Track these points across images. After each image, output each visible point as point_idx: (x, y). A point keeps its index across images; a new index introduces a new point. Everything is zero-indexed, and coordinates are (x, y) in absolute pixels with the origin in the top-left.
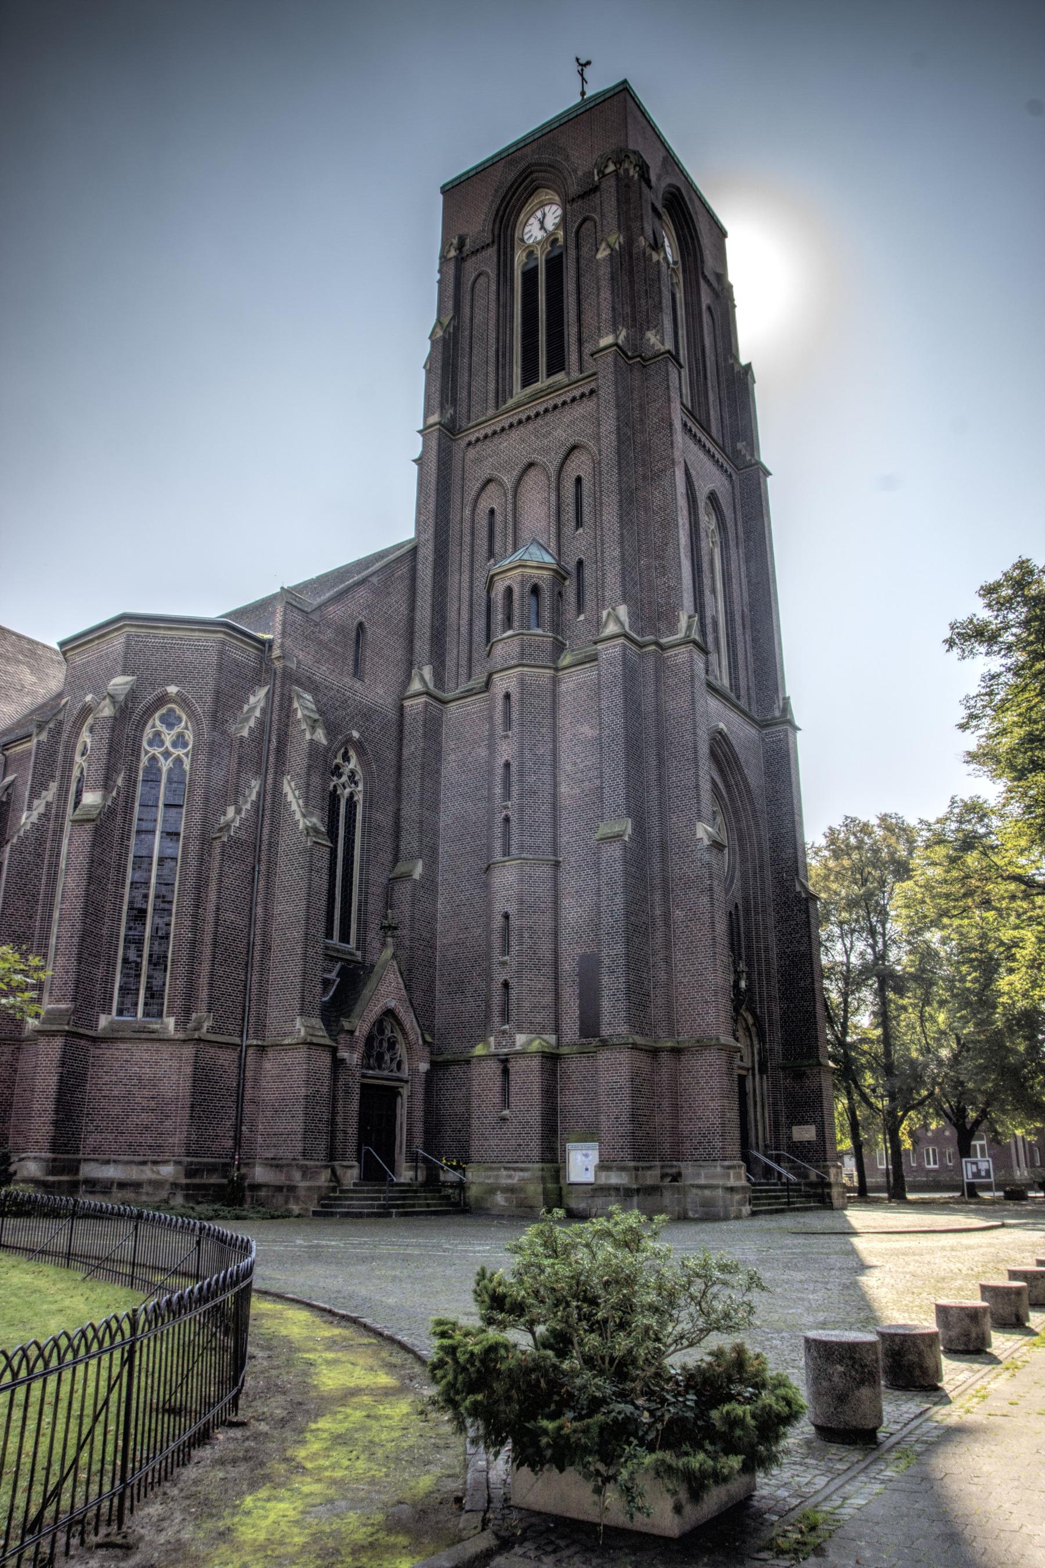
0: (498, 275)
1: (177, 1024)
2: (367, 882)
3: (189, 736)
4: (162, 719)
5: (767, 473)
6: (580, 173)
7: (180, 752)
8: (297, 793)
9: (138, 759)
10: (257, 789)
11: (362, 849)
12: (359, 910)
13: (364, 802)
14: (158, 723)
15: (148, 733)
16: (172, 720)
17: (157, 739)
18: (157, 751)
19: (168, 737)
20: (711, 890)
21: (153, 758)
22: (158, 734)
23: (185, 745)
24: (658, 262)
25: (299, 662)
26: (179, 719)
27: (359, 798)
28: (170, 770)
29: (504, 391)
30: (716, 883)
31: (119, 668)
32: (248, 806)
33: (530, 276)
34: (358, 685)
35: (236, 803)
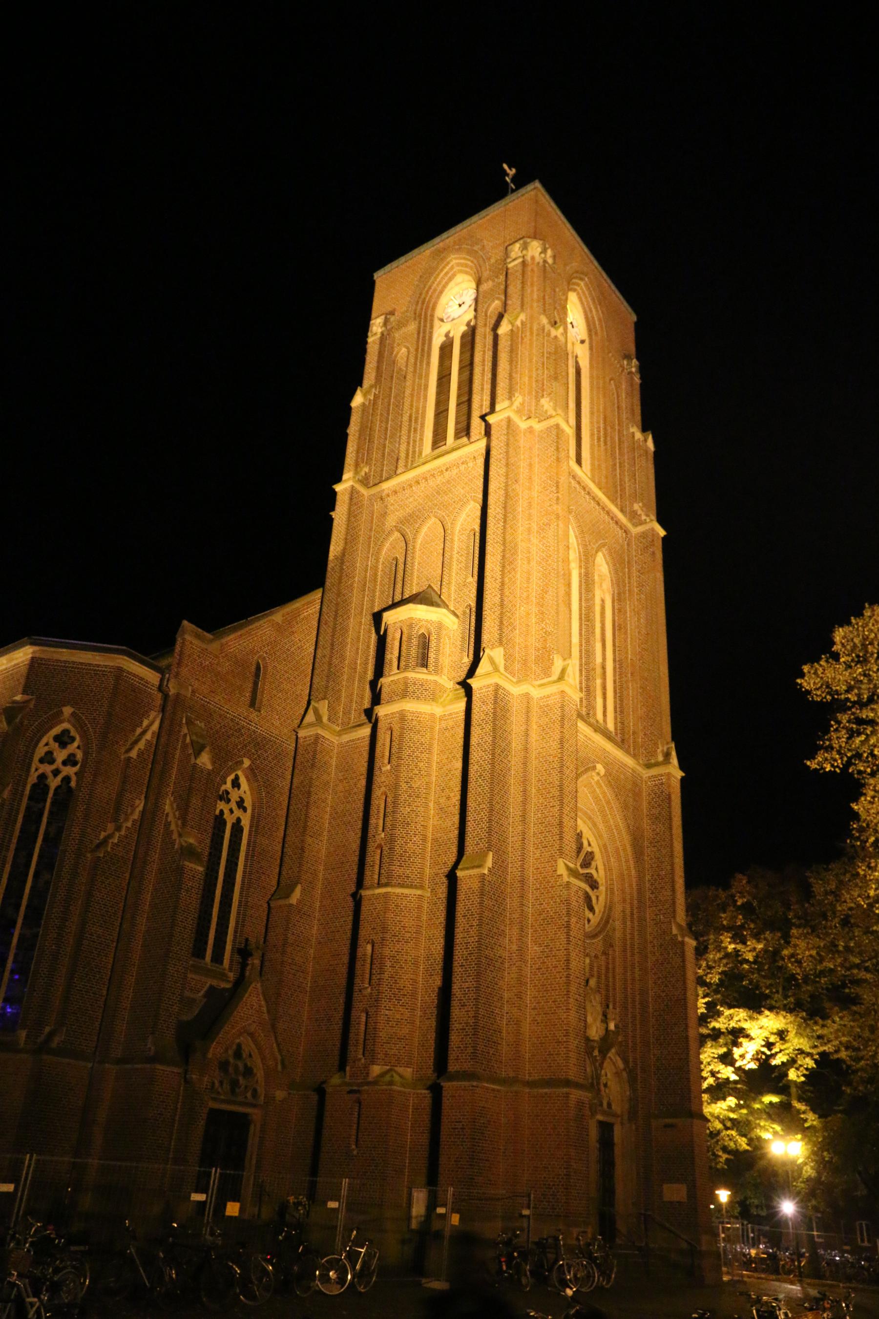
0: (417, 350)
1: (28, 1036)
2: (246, 905)
3: (79, 756)
4: (57, 738)
5: (361, 386)
6: (493, 261)
7: (70, 771)
8: (177, 813)
9: (28, 775)
10: (141, 808)
11: (244, 872)
12: (236, 932)
13: (251, 827)
14: (51, 741)
15: (41, 751)
16: (65, 739)
17: (48, 758)
18: (47, 769)
19: (61, 755)
20: (568, 926)
21: (222, 811)
22: (50, 753)
23: (75, 764)
24: (556, 337)
25: (193, 691)
26: (73, 739)
27: (246, 823)
28: (58, 788)
29: (414, 452)
30: (574, 920)
31: (20, 689)
32: (129, 824)
33: (446, 349)
34: (254, 715)
35: (115, 820)
